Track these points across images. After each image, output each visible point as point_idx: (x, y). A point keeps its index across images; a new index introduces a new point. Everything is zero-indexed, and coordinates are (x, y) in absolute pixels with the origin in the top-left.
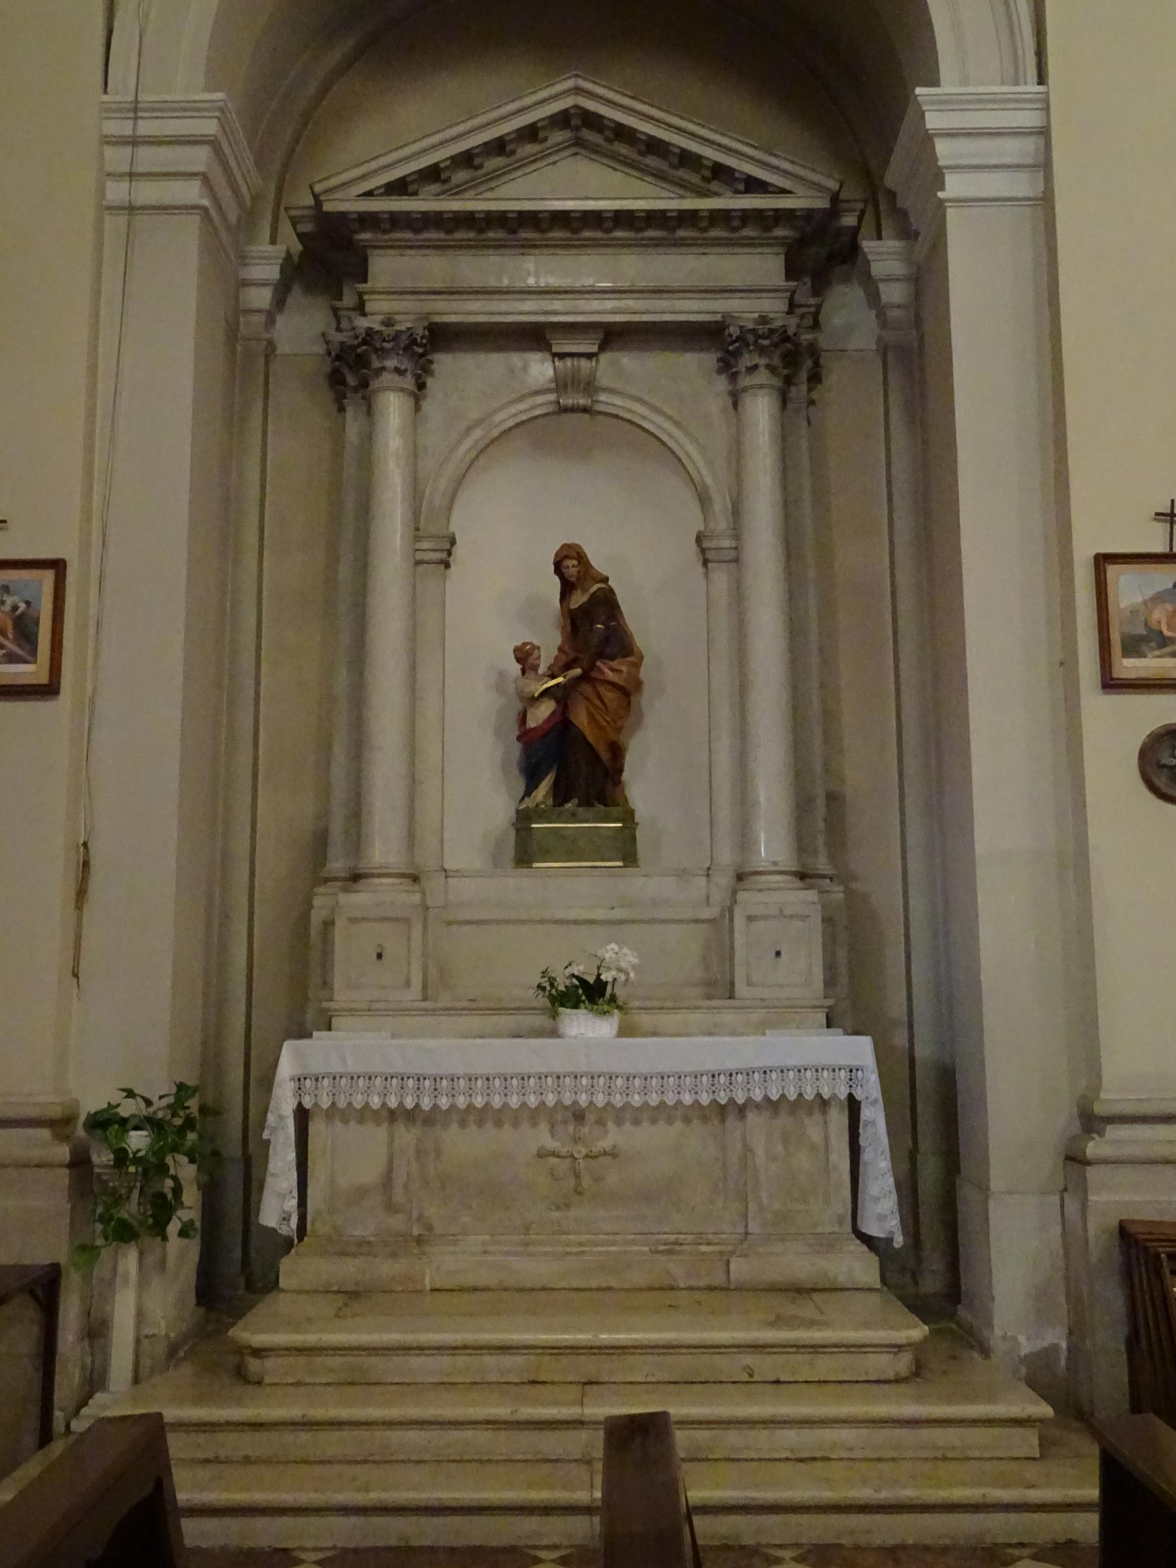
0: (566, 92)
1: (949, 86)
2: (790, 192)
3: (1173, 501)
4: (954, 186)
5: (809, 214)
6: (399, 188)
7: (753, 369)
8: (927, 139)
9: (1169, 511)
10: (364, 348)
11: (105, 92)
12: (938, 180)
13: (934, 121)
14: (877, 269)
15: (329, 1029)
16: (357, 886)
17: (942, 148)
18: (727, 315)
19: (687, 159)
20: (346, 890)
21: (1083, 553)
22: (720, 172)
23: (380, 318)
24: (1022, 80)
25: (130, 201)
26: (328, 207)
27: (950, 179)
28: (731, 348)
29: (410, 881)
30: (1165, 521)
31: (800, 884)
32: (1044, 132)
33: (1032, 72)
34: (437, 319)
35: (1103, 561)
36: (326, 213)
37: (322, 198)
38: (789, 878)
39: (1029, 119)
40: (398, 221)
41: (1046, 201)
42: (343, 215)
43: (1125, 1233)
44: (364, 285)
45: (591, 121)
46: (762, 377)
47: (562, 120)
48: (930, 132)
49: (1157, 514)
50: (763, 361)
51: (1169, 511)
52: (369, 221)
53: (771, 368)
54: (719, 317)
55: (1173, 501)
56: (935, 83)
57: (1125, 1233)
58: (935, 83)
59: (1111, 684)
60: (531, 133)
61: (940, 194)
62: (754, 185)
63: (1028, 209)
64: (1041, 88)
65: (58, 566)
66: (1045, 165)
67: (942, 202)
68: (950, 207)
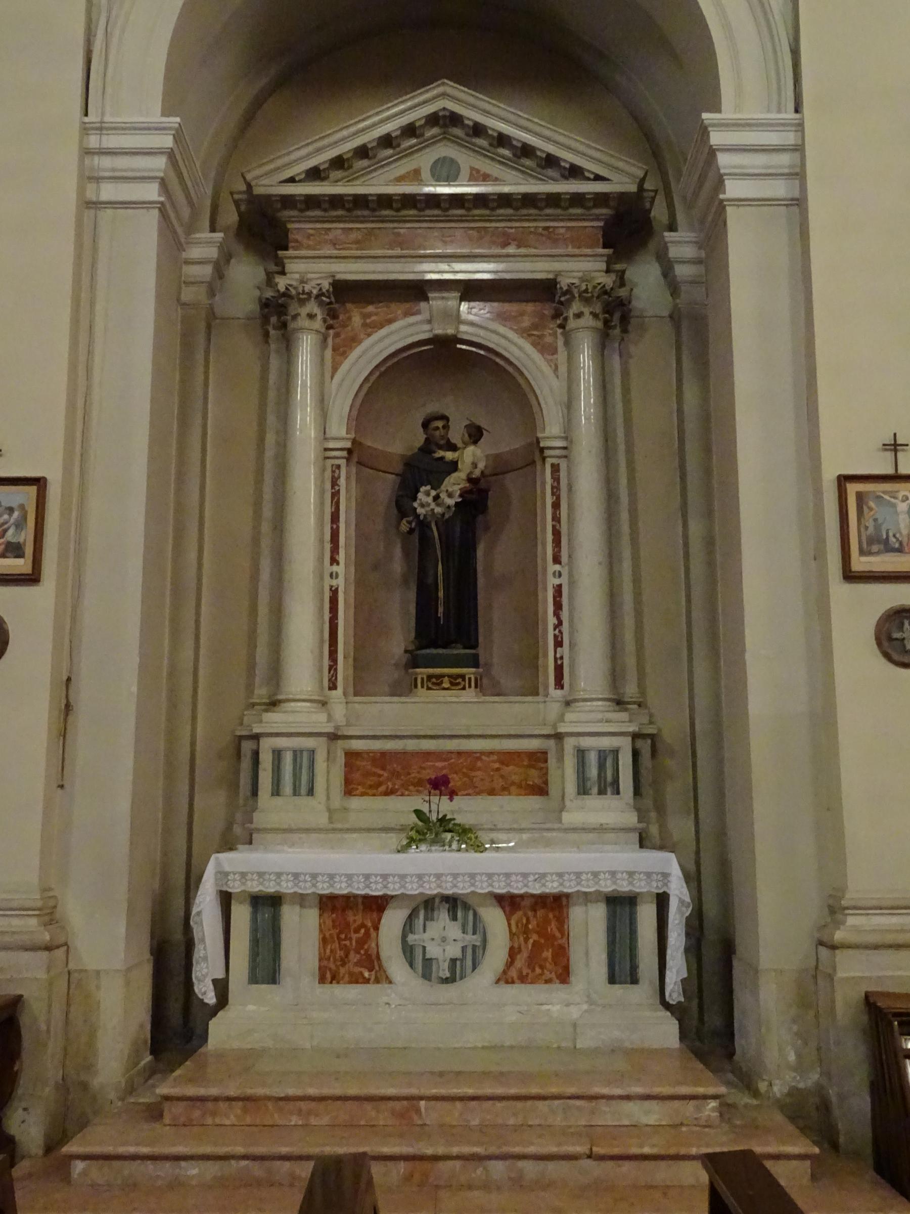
0: (434, 98)
1: (728, 113)
2: (608, 180)
3: (895, 434)
4: (733, 189)
5: (622, 196)
6: (315, 174)
7: (579, 315)
8: (712, 153)
9: (893, 442)
10: (283, 299)
11: (86, 115)
12: (720, 184)
13: (716, 138)
14: (674, 252)
15: (251, 843)
16: (276, 709)
17: (724, 160)
18: (558, 273)
19: (526, 151)
20: (266, 711)
21: (830, 474)
22: (551, 161)
23: (297, 276)
24: (783, 110)
25: (397, 475)
26: (258, 191)
27: (729, 184)
28: (563, 299)
29: (320, 705)
30: (891, 450)
31: (617, 708)
32: (799, 149)
33: (791, 106)
34: (339, 277)
35: (844, 480)
36: (258, 196)
37: (253, 183)
38: (608, 703)
39: (790, 138)
40: (312, 202)
41: (799, 203)
42: (269, 197)
43: (870, 1003)
44: (285, 252)
45: (455, 119)
46: (587, 320)
47: (433, 119)
48: (714, 147)
49: (884, 445)
50: (586, 311)
51: (893, 442)
52: (288, 201)
53: (595, 315)
54: (551, 276)
55: (895, 434)
56: (719, 111)
57: (870, 1003)
58: (719, 111)
59: (850, 576)
60: (410, 130)
61: (721, 196)
62: (575, 172)
63: (783, 181)
64: (797, 116)
65: (39, 482)
66: (799, 175)
67: (722, 201)
68: (729, 205)
